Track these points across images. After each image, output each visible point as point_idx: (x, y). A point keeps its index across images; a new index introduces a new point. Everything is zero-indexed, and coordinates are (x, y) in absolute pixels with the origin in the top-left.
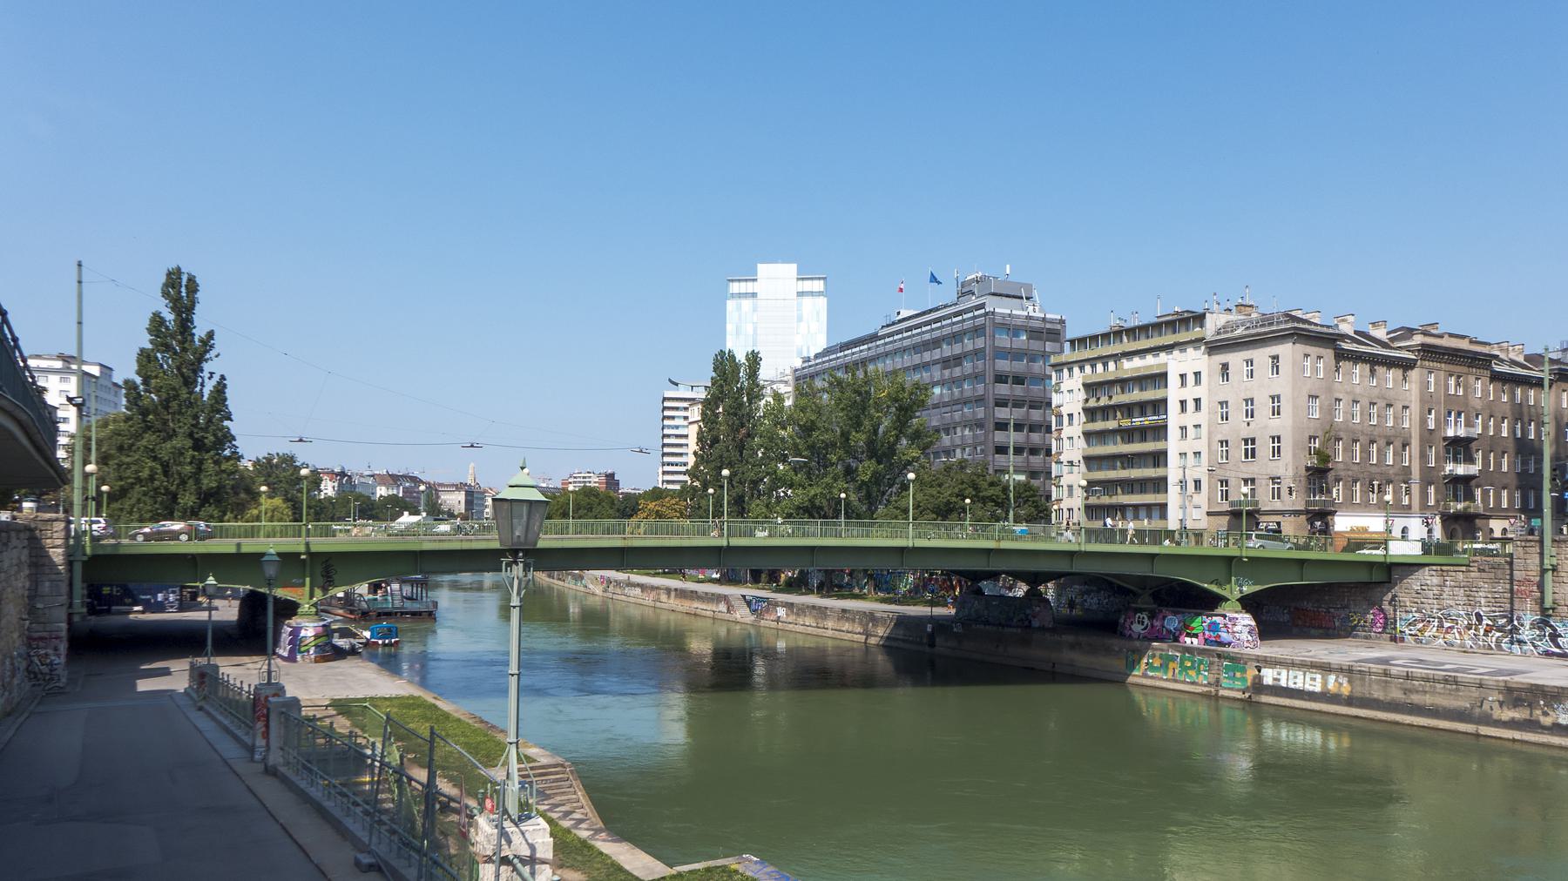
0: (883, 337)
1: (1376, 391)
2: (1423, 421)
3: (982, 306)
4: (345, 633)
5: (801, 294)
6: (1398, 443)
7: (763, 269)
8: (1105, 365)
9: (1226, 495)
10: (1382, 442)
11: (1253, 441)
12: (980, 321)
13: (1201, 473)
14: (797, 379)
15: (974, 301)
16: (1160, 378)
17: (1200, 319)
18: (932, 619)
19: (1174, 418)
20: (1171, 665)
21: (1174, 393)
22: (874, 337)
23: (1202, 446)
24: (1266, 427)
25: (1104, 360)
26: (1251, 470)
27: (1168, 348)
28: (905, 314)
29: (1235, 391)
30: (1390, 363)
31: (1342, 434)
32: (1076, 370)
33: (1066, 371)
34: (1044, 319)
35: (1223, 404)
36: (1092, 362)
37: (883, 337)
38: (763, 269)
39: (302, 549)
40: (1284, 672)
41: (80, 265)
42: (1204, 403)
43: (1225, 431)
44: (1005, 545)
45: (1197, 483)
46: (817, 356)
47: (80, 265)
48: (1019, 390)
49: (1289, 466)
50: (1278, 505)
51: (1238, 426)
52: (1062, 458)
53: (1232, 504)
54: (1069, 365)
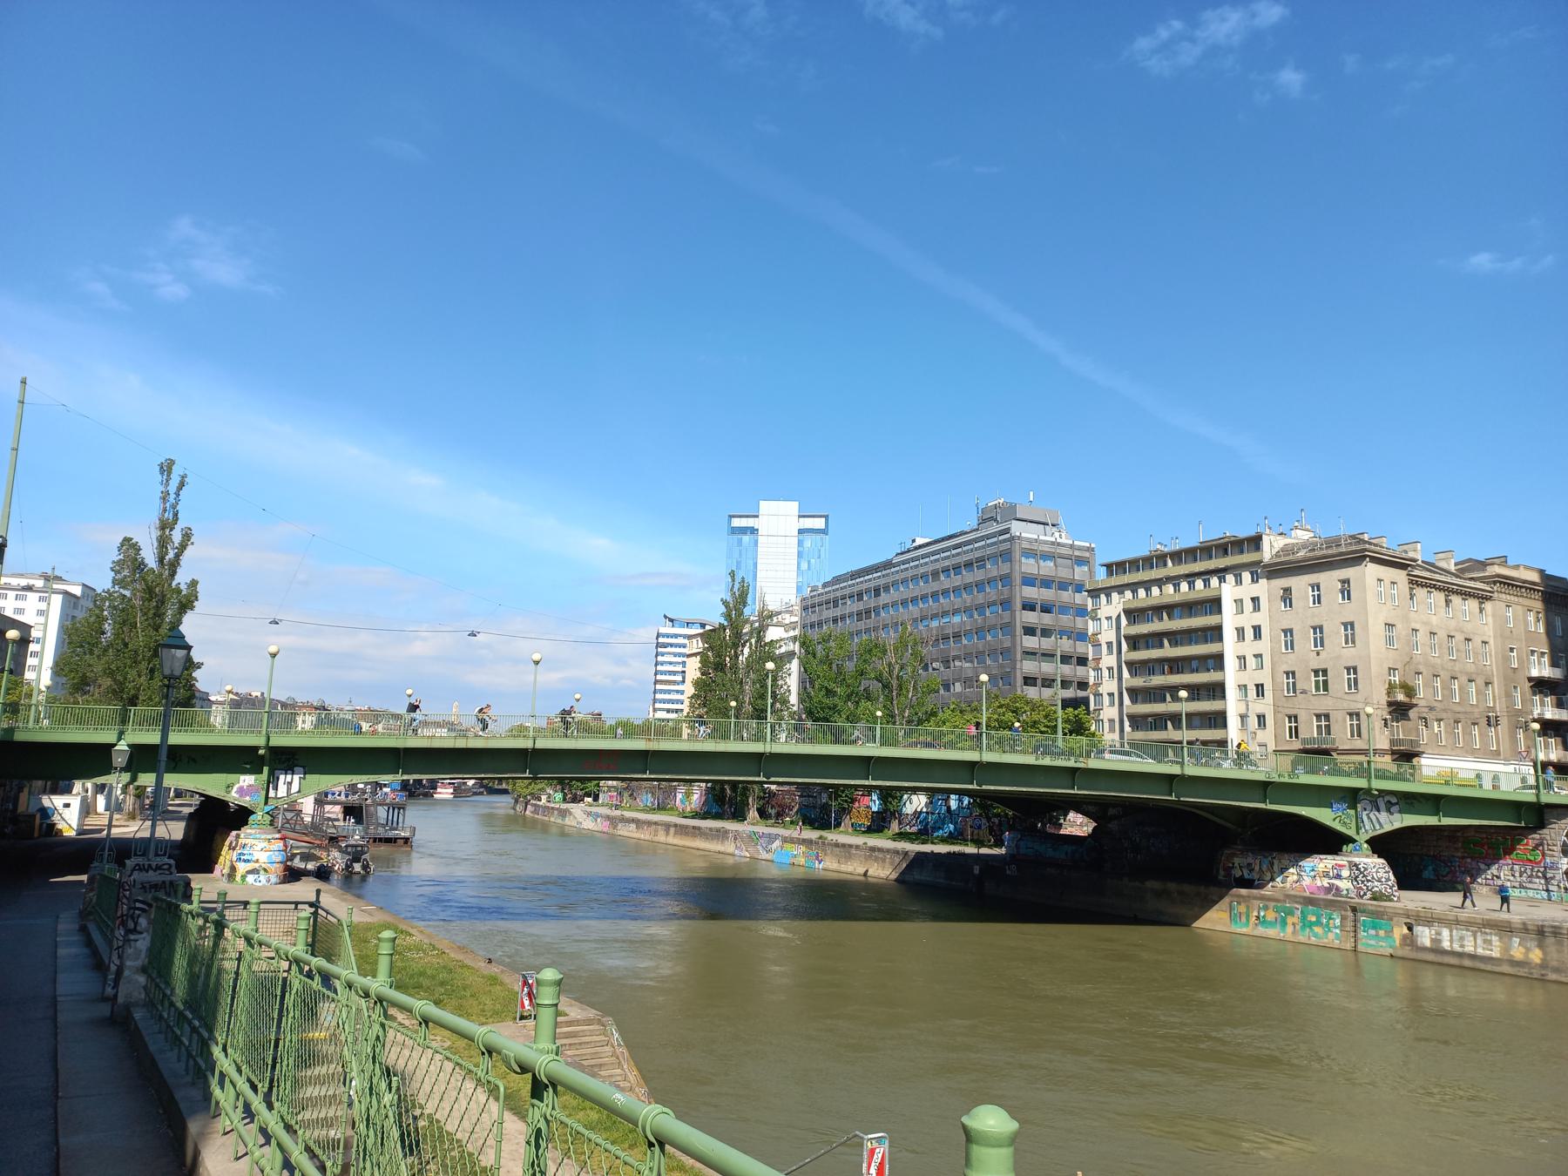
0: (898, 564)
1: (1453, 623)
2: (1507, 659)
3: (1007, 531)
4: (306, 857)
5: (801, 531)
6: (1480, 681)
7: (764, 506)
8: (1148, 590)
9: (1295, 732)
10: (1464, 679)
11: (1325, 672)
12: (1006, 546)
13: (1265, 706)
14: (805, 609)
15: (995, 528)
16: (1215, 604)
17: (1255, 542)
18: (977, 858)
19: (1230, 647)
20: (1290, 920)
21: (1229, 620)
22: (888, 565)
23: (1264, 677)
24: (1339, 657)
25: (1147, 584)
26: (1323, 704)
27: (1220, 573)
28: (920, 541)
29: (1303, 614)
30: (1466, 594)
31: (1421, 668)
32: (1115, 595)
33: (1103, 596)
34: (1072, 546)
35: (1288, 632)
36: (1133, 587)
37: (898, 564)
38: (764, 506)
39: (261, 742)
40: (1446, 933)
41: (24, 382)
42: (1265, 632)
43: (1290, 662)
44: (1093, 763)
45: (1261, 719)
46: (825, 585)
47: (24, 382)
48: (1047, 619)
49: (1374, 704)
50: (1359, 744)
51: (1305, 655)
52: (1100, 690)
53: (1304, 741)
54: (1108, 591)
